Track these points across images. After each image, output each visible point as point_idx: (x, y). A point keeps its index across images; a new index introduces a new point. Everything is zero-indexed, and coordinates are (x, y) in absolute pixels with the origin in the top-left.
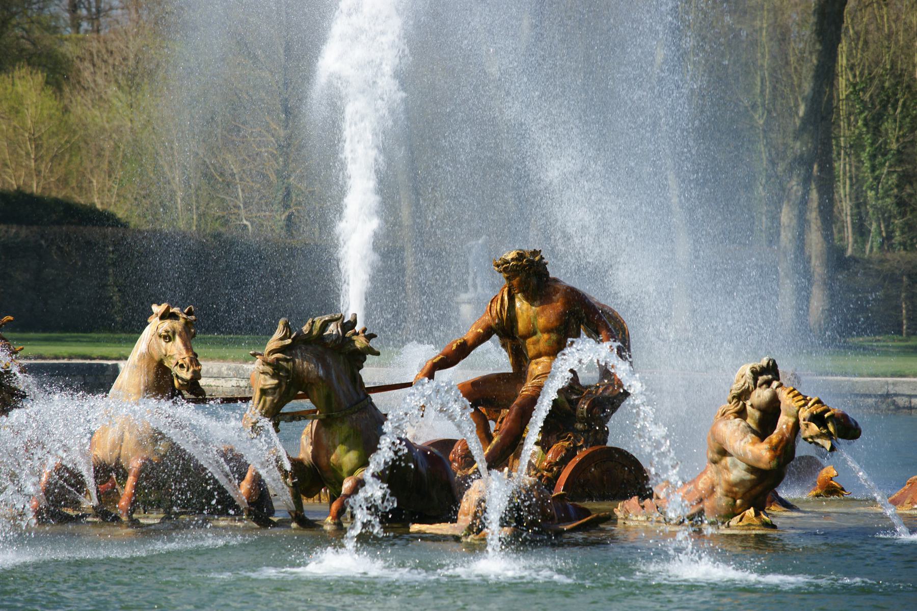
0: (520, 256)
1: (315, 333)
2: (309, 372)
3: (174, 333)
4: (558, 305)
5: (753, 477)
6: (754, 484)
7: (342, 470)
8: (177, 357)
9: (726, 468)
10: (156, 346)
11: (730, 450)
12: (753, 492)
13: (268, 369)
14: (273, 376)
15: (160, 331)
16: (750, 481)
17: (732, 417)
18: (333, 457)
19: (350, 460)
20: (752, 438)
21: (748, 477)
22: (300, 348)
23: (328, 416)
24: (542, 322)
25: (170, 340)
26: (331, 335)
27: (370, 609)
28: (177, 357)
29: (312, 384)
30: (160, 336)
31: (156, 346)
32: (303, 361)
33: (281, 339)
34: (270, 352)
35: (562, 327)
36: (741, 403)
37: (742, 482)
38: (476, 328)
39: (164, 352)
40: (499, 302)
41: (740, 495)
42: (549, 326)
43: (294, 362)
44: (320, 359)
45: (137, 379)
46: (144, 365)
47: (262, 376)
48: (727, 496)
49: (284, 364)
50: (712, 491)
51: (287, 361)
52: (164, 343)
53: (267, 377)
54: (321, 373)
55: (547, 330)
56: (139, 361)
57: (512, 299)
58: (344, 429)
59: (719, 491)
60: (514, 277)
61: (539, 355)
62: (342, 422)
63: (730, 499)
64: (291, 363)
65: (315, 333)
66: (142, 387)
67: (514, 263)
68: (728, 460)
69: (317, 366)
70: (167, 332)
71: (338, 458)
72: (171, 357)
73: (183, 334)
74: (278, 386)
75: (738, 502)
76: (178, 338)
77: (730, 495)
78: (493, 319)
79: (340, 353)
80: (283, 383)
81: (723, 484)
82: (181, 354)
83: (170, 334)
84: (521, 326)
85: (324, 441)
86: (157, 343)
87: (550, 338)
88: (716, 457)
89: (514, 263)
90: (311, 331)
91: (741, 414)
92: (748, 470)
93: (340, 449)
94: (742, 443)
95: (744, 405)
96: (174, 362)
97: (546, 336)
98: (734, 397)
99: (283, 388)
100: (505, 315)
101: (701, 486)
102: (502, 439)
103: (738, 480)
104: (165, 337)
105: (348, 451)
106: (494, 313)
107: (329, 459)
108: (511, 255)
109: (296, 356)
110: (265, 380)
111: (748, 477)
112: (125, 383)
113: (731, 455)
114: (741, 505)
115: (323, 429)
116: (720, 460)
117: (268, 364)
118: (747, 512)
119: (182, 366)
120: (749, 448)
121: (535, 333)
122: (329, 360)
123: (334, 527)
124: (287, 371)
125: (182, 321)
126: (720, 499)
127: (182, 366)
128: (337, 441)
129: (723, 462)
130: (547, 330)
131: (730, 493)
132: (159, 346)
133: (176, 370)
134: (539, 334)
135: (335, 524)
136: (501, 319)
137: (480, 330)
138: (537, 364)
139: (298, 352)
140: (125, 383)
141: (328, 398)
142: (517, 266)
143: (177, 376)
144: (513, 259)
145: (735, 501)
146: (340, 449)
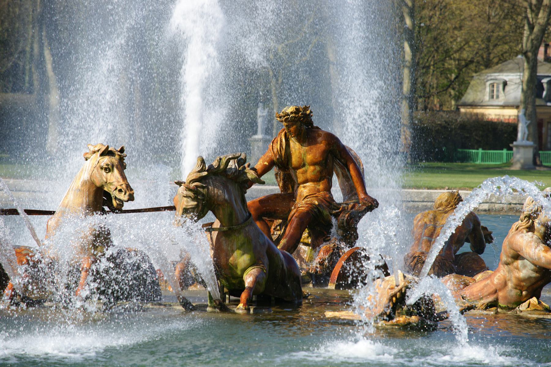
0: (297, 111)
1: (222, 167)
2: (218, 196)
3: (113, 166)
4: (321, 146)
5: (538, 275)
6: (537, 280)
7: (237, 268)
8: (115, 183)
9: (517, 268)
10: (98, 176)
11: (525, 256)
12: (535, 286)
13: (191, 194)
14: (193, 200)
15: (102, 164)
16: (535, 278)
17: (525, 231)
18: (231, 259)
19: (244, 261)
20: (544, 247)
21: (534, 275)
22: (211, 178)
23: (230, 229)
24: (309, 158)
25: (110, 171)
26: (231, 169)
27: (161, 365)
28: (115, 183)
29: (219, 205)
30: (102, 168)
31: (98, 176)
32: (214, 188)
33: (199, 172)
34: (190, 181)
35: (324, 162)
36: (531, 221)
37: (530, 278)
38: (263, 162)
39: (105, 180)
40: (279, 143)
41: (525, 288)
42: (315, 160)
43: (208, 189)
44: (225, 187)
45: (80, 200)
46: (86, 189)
47: (185, 199)
48: (516, 288)
49: (201, 190)
50: (505, 284)
51: (203, 187)
52: (104, 174)
53: (189, 200)
54: (227, 197)
55: (314, 164)
56: (82, 186)
57: (287, 140)
58: (240, 238)
59: (510, 285)
60: (292, 125)
61: (306, 181)
62: (239, 233)
63: (518, 291)
64: (206, 190)
65: (222, 167)
66: (85, 206)
67: (293, 115)
68: (519, 263)
69: (223, 192)
70: (107, 165)
71: (235, 259)
72: (111, 184)
73: (119, 166)
74: (197, 206)
75: (524, 293)
76: (115, 170)
77: (519, 288)
78: (275, 156)
79: (236, 182)
80: (200, 205)
81: (514, 280)
82: (118, 182)
83: (110, 167)
84: (295, 160)
85: (224, 247)
86: (99, 173)
87: (315, 169)
88: (510, 260)
89: (293, 115)
90: (219, 166)
91: (531, 229)
92: (534, 271)
93: (237, 253)
94: (537, 251)
95: (533, 222)
96: (113, 187)
97: (312, 168)
98: (525, 217)
99: (200, 208)
100: (283, 152)
101: (496, 281)
102: (287, 242)
103: (526, 277)
104: (106, 169)
105: (243, 254)
106: (275, 150)
107: (228, 260)
108: (290, 109)
109: (209, 184)
110: (187, 202)
111: (534, 275)
112: (70, 203)
113: (523, 258)
114: (526, 296)
115: (223, 238)
116: (513, 262)
117: (190, 190)
118: (531, 300)
119: (120, 191)
120: (542, 254)
121: (304, 165)
122: (230, 187)
123: (245, 311)
124: (203, 195)
125: (117, 157)
126: (511, 291)
127: (120, 191)
128: (235, 247)
129: (515, 264)
130: (314, 164)
131: (519, 286)
132: (101, 176)
133: (116, 194)
134: (307, 167)
135: (246, 309)
136: (281, 156)
137: (266, 163)
138: (304, 187)
139: (210, 181)
140: (70, 203)
141: (231, 215)
142: (295, 117)
143: (116, 198)
144: (292, 113)
145: (522, 293)
146: (237, 253)
